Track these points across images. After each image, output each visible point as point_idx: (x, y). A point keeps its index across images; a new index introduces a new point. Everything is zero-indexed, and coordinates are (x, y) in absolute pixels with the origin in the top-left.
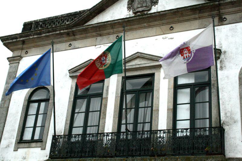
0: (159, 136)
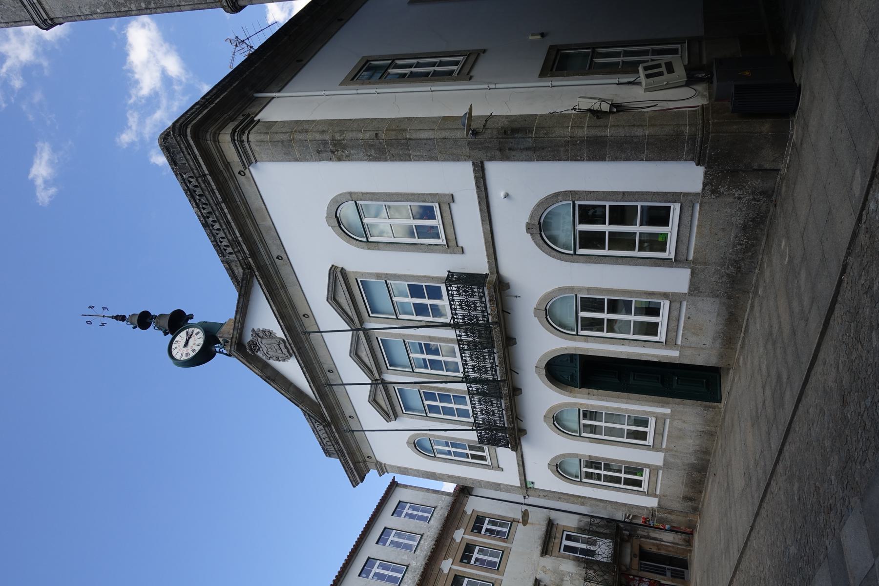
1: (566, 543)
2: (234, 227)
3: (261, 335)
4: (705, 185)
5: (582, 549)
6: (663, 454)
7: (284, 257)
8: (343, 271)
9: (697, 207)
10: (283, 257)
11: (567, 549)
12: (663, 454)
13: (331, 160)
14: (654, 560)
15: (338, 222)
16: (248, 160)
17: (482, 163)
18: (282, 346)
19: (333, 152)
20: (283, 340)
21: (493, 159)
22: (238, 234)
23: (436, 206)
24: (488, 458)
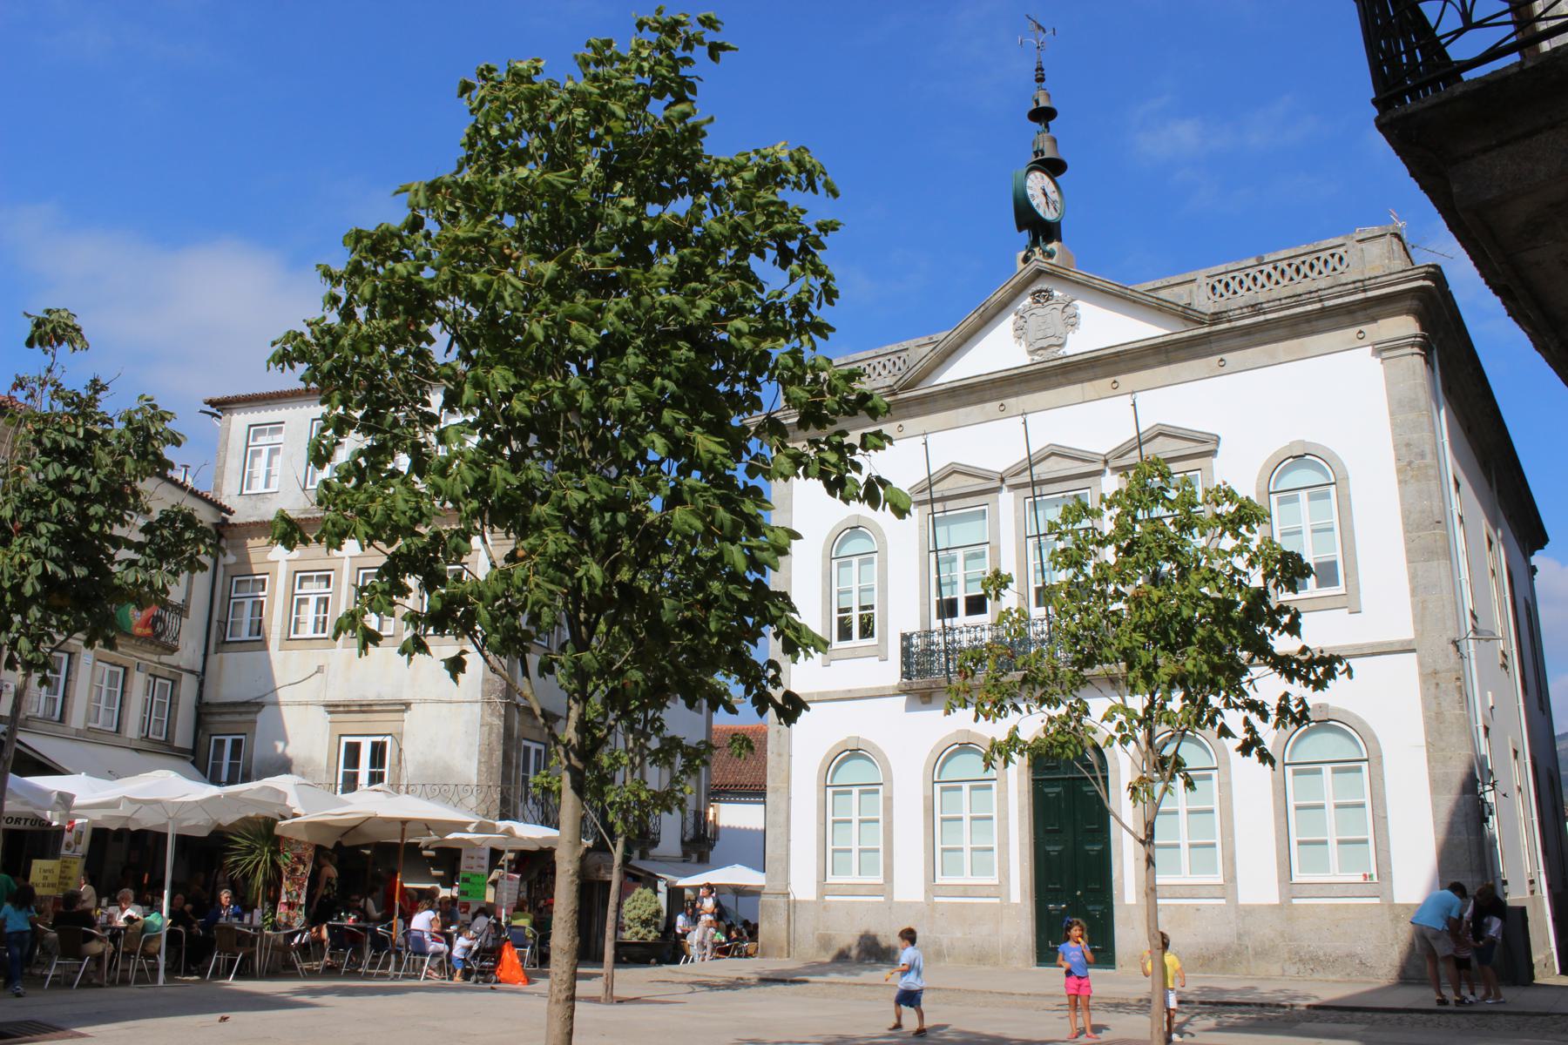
1: (228, 741)
2: (1282, 314)
3: (1069, 310)
5: (220, 767)
6: (813, 897)
7: (1224, 370)
8: (1212, 453)
9: (1377, 901)
10: (1222, 369)
11: (353, 751)
12: (813, 897)
13: (1398, 460)
14: (107, 894)
15: (1299, 458)
16: (1380, 349)
17: (1413, 651)
18: (1053, 341)
19: (1410, 463)
20: (1061, 346)
21: (1421, 664)
22: (1269, 316)
23: (1340, 589)
24: (846, 644)
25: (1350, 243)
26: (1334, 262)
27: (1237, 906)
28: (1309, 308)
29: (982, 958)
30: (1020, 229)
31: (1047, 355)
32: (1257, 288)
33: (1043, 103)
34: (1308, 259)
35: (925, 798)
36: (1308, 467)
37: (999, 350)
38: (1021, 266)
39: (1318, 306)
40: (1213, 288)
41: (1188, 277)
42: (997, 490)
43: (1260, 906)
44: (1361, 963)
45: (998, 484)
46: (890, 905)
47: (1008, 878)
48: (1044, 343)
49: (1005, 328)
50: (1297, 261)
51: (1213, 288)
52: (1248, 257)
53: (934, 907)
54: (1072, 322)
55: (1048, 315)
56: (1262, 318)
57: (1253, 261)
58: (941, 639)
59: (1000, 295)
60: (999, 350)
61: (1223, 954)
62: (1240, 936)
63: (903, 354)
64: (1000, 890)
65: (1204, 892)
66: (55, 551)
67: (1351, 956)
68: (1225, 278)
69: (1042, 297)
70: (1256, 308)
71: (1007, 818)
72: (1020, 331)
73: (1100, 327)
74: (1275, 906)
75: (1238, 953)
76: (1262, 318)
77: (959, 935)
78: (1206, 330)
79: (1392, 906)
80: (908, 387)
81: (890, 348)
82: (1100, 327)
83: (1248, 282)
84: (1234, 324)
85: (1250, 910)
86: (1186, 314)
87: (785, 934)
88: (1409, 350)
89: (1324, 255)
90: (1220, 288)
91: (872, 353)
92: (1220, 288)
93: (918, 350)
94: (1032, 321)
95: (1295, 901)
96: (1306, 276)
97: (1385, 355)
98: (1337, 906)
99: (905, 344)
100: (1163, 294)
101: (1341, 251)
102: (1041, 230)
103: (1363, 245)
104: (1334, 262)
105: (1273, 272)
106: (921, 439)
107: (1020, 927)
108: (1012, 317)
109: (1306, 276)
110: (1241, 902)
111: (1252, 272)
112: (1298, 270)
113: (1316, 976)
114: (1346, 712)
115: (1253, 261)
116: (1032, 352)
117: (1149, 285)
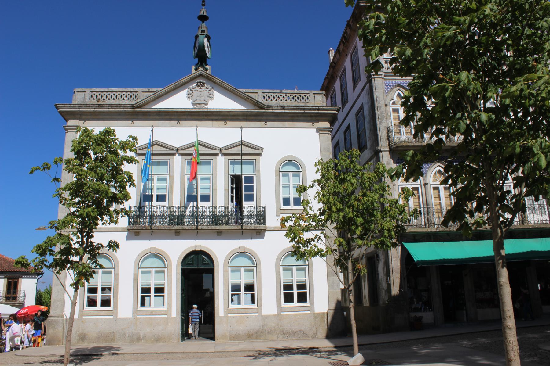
0: (220, 210)
2: (312, 111)
4: (319, 314)
8: (260, 154)
9: (309, 312)
16: (319, 130)
18: (203, 102)
25: (311, 94)
26: (305, 98)
27: (262, 316)
28: (300, 111)
29: (158, 339)
30: (196, 57)
31: (201, 106)
32: (280, 100)
33: (205, 14)
34: (297, 95)
35: (134, 274)
36: (293, 165)
37: (180, 101)
38: (194, 71)
39: (303, 111)
40: (92, 96)
41: (84, 90)
42: (174, 154)
43: (270, 315)
44: (304, 333)
45: (175, 152)
46: (116, 320)
47: (171, 307)
48: (200, 102)
49: (184, 93)
50: (294, 95)
51: (92, 96)
52: (277, 89)
53: (137, 319)
54: (211, 97)
55: (202, 92)
56: (284, 111)
57: (278, 91)
58: (177, 210)
59: (184, 80)
60: (180, 101)
61: (256, 333)
62: (263, 326)
63: (136, 94)
64: (167, 312)
65: (250, 311)
66: (408, 88)
67: (300, 331)
68: (268, 95)
69: (200, 84)
70: (283, 107)
71: (171, 283)
72: (189, 96)
73: (221, 102)
74: (275, 315)
75: (262, 332)
76: (284, 111)
77: (148, 330)
78: (264, 111)
79: (314, 313)
80: (140, 106)
81: (129, 90)
82: (221, 102)
83: (276, 98)
84: (81, 110)
85: (267, 317)
86: (257, 104)
87: (62, 334)
88: (328, 132)
89: (302, 95)
90: (266, 97)
91: (121, 90)
92: (266, 97)
93: (143, 94)
94: (195, 92)
95: (282, 313)
96: (296, 101)
97: (320, 132)
98: (296, 315)
99: (137, 89)
100: (250, 95)
101: (308, 95)
102: (202, 58)
103: (316, 95)
104: (305, 98)
105: (108, 95)
106: (151, 129)
107: (176, 327)
108: (187, 90)
109: (296, 101)
110: (316, 312)
111: (278, 95)
112: (293, 98)
113: (289, 338)
114: (165, 253)
115: (278, 91)
116: (193, 104)
117: (247, 90)
